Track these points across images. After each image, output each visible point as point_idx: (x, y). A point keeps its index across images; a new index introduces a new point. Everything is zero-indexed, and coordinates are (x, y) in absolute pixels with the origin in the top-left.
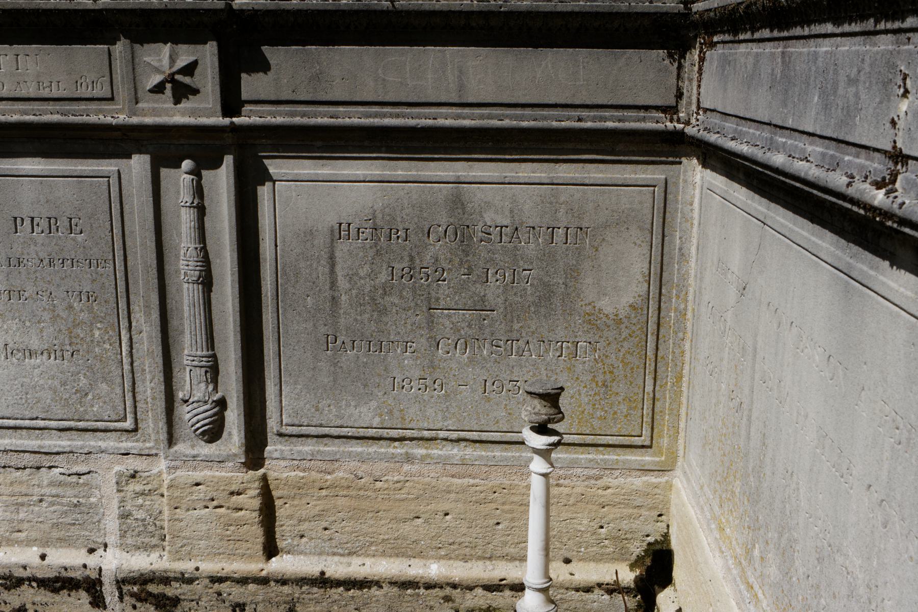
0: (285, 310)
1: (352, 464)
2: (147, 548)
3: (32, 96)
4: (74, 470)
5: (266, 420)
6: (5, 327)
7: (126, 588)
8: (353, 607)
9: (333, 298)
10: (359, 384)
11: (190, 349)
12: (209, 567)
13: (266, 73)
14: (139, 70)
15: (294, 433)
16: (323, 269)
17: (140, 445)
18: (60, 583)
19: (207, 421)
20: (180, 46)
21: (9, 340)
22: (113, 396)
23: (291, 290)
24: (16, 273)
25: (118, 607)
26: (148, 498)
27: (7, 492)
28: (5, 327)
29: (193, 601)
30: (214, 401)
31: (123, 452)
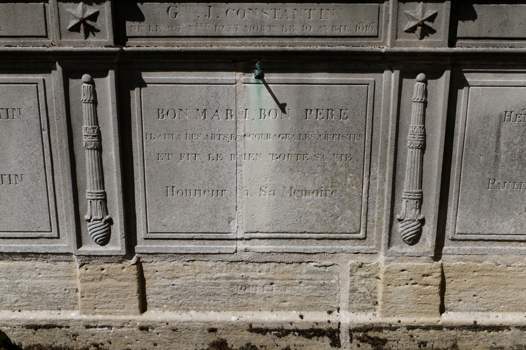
0: (466, 164)
1: (495, 256)
2: (364, 310)
3: (328, 34)
4: (324, 264)
5: (445, 230)
6: (292, 177)
7: (354, 334)
8: (492, 342)
9: (496, 157)
10: (505, 208)
12: (407, 320)
13: (474, 21)
14: (400, 18)
15: (462, 238)
16: (492, 139)
17: (367, 247)
18: (314, 333)
20: (427, 3)
21: (294, 185)
22: (354, 218)
23: (471, 152)
24: (304, 143)
25: (349, 345)
26: (368, 279)
27: (280, 278)
28: (292, 177)
29: (395, 341)
30: (419, 220)
31: (356, 252)
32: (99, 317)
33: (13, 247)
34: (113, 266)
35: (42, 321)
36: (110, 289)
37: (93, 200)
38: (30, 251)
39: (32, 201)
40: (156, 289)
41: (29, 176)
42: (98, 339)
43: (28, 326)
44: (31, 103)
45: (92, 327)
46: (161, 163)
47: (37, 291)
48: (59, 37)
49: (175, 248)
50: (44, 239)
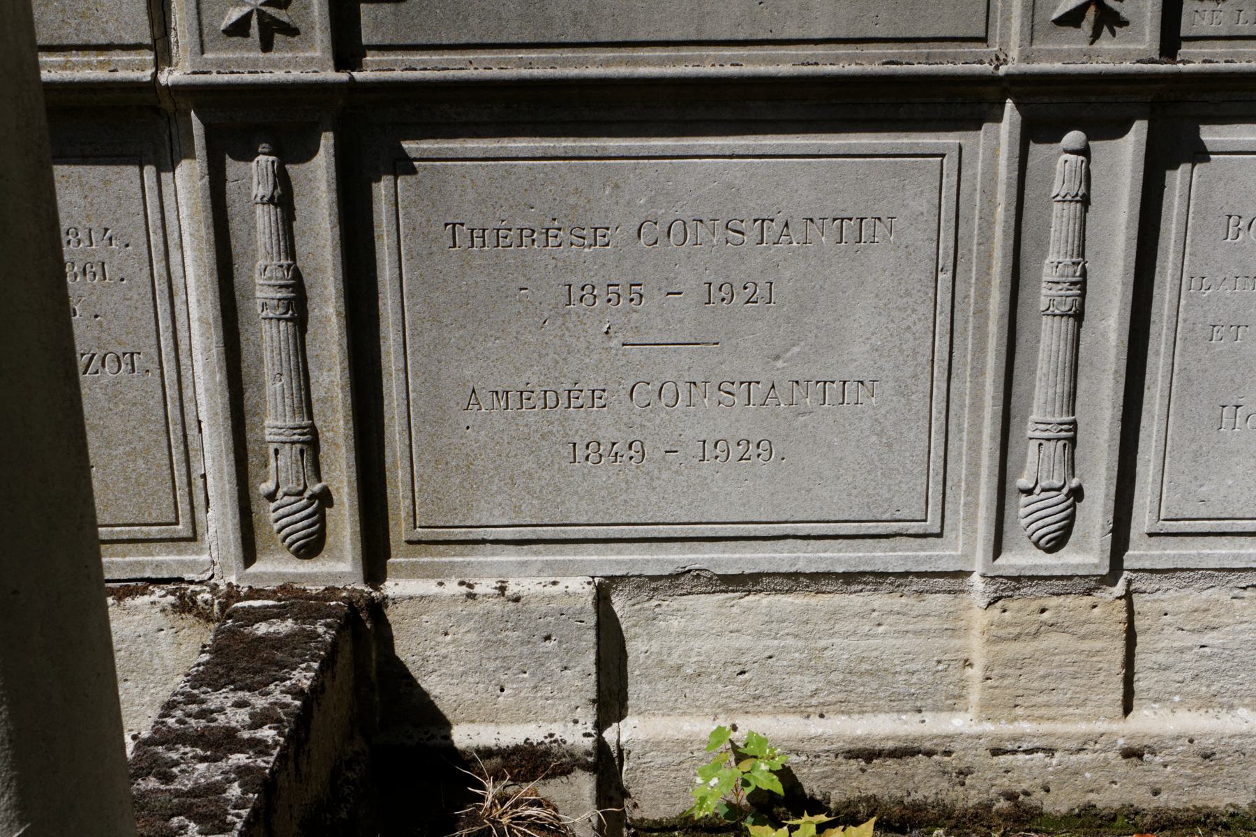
11: (1041, 408)
19: (305, 523)
32: (1026, 727)
33: (827, 559)
34: (1070, 601)
35: (888, 738)
36: (1057, 658)
37: (1049, 440)
38: (868, 569)
39: (890, 445)
40: (1160, 658)
41: (891, 384)
42: (1018, 781)
43: (849, 751)
44: (922, 204)
45: (1006, 752)
46: (1218, 349)
47: (869, 667)
48: (1029, 38)
49: (1221, 557)
50: (904, 539)
